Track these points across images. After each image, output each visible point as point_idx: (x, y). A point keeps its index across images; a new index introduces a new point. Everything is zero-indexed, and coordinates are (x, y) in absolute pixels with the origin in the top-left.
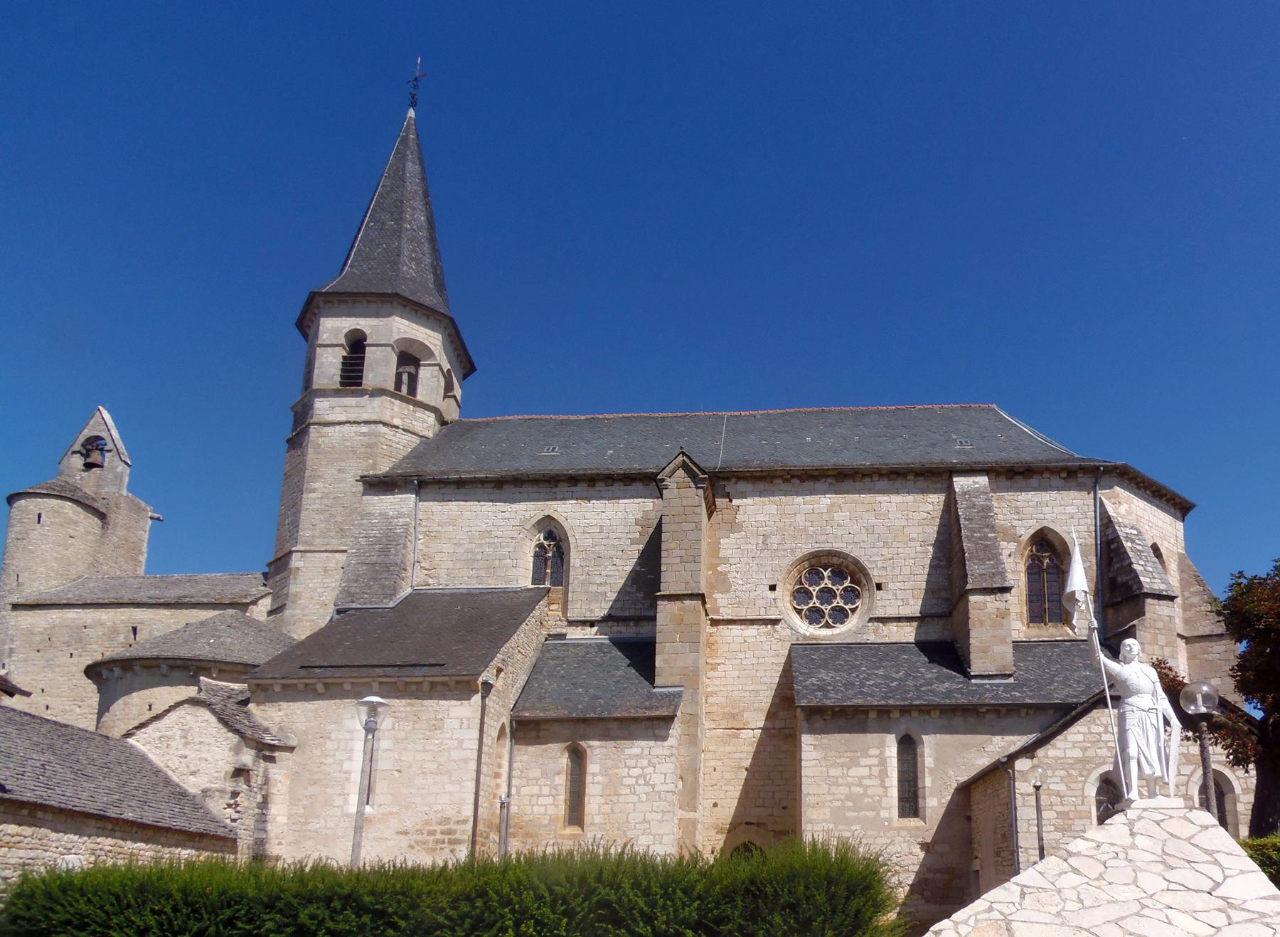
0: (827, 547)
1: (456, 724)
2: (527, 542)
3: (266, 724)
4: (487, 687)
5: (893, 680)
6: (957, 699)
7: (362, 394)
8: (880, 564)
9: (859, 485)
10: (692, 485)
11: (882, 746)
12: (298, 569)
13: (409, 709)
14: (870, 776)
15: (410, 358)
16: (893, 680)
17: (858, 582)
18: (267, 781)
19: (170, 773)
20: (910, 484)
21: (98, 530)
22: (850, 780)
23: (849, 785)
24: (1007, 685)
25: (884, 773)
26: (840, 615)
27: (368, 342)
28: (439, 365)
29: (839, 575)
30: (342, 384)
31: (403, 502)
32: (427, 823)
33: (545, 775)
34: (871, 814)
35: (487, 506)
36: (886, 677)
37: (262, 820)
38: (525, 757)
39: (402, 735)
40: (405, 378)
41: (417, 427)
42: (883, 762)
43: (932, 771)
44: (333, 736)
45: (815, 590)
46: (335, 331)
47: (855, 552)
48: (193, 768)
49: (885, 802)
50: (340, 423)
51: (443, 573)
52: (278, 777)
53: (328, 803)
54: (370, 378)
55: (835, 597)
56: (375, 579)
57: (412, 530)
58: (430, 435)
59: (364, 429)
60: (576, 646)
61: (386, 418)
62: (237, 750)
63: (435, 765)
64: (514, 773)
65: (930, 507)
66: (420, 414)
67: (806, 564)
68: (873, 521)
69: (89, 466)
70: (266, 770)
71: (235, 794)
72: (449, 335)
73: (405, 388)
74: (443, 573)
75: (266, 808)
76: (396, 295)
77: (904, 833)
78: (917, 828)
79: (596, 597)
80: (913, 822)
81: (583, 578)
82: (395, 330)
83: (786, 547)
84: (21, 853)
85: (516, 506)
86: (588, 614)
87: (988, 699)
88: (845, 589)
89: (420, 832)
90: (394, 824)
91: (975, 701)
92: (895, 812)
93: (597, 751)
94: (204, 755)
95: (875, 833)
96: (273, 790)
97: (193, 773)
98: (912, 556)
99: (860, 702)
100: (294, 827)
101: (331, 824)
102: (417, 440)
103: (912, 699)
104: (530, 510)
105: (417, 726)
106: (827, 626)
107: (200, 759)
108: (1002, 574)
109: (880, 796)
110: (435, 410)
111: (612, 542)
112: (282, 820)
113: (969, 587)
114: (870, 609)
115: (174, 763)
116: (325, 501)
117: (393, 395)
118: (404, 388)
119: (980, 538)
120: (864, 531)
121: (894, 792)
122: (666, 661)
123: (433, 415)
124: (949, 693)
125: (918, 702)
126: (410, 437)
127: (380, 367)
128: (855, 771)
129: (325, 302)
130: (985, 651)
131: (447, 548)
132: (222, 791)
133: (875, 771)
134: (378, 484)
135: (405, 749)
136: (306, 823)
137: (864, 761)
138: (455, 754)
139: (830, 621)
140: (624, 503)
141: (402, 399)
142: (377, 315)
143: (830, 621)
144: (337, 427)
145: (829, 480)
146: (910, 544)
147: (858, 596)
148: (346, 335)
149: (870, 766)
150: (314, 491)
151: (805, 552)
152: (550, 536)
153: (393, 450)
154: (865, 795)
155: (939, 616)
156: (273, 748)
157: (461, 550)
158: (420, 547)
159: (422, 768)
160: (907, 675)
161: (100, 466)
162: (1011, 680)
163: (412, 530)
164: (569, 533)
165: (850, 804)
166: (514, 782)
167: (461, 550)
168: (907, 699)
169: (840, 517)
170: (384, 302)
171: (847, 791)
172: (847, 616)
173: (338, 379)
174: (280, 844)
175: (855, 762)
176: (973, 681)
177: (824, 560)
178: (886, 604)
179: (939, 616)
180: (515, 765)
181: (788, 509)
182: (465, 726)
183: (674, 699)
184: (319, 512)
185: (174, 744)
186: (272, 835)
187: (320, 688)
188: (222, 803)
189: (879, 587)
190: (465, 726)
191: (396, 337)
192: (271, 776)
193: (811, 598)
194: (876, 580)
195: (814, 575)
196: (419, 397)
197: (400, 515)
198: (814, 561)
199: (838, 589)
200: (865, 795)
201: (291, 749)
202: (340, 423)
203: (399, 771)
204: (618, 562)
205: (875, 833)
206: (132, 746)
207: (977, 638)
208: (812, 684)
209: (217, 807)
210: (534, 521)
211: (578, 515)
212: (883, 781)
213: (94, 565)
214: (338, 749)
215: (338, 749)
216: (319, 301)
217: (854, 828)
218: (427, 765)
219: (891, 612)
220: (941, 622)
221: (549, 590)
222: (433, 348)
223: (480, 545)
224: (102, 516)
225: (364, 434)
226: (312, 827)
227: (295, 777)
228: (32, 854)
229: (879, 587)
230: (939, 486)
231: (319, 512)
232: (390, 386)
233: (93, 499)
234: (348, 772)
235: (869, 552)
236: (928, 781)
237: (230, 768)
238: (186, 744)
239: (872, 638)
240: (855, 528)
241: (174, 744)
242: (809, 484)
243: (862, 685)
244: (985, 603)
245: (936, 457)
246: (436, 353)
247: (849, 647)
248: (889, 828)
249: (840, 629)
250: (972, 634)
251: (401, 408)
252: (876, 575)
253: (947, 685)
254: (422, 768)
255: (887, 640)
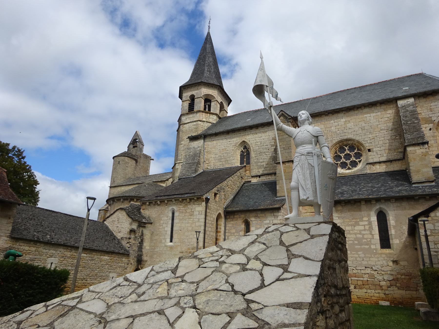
0: (345, 138)
1: (197, 213)
2: (238, 151)
3: (145, 215)
4: (207, 200)
5: (375, 187)
6: (404, 193)
7: (194, 113)
8: (369, 141)
9: (356, 112)
10: (286, 121)
11: (369, 216)
12: (177, 168)
13: (183, 208)
14: (365, 230)
15: (208, 100)
16: (375, 187)
17: (361, 150)
18: (142, 234)
19: (114, 232)
20: (378, 108)
21: (134, 165)
22: (356, 231)
23: (356, 234)
24: (431, 186)
25: (371, 228)
26: (354, 164)
27: (196, 97)
28: (217, 101)
29: (352, 148)
30: (189, 111)
31: (200, 143)
32: (189, 249)
33: (237, 232)
34: (367, 247)
35: (225, 141)
36: (372, 187)
37: (140, 247)
38: (230, 225)
39: (181, 218)
40: (207, 106)
41: (211, 120)
42: (370, 223)
43: (394, 227)
44: (162, 219)
45: (342, 155)
46: (187, 96)
47: (357, 138)
48: (119, 230)
49: (373, 241)
50: (188, 123)
51: (212, 164)
52: (147, 233)
53: (161, 242)
54: (196, 108)
55: (351, 157)
56: (190, 168)
57: (202, 151)
58: (215, 122)
59: (195, 123)
60: (253, 185)
61: (200, 120)
62: (131, 224)
63: (190, 228)
64: (226, 231)
65: (389, 115)
66: (211, 116)
67: (338, 145)
68: (364, 125)
69: (134, 147)
70: (142, 231)
71: (130, 238)
72: (219, 89)
73: (207, 109)
74: (212, 164)
75: (142, 244)
76: (202, 82)
77: (384, 256)
78: (390, 254)
79: (260, 167)
80: (387, 251)
81: (256, 161)
82: (202, 92)
83: (328, 140)
84: (31, 256)
85: (233, 140)
86: (258, 173)
87: (420, 192)
88: (355, 153)
89: (186, 252)
90: (179, 249)
91: (412, 193)
92: (379, 246)
93: (254, 222)
94: (122, 226)
95: (369, 255)
96: (145, 238)
97: (119, 232)
98: (383, 136)
99: (356, 197)
100: (151, 250)
101: (161, 249)
102: (210, 124)
103: (381, 195)
104: (236, 140)
105: (186, 214)
106: (349, 169)
107: (122, 228)
108: (423, 137)
109: (371, 239)
110: (216, 114)
111: (265, 147)
112: (147, 248)
113: (406, 144)
114: (367, 159)
115: (115, 229)
116: (185, 147)
117: (202, 112)
118: (207, 110)
119: (410, 124)
120: (360, 129)
121: (377, 237)
122: (280, 187)
123: (215, 116)
124: (399, 192)
125: (383, 196)
126: (208, 124)
127: (200, 104)
128: (357, 228)
129: (184, 89)
130: (418, 171)
131: (213, 156)
132: (126, 238)
133: (367, 227)
134: (193, 139)
135: (183, 223)
136: (155, 249)
137: (361, 223)
138: (197, 224)
139: (350, 167)
140: (267, 134)
141: (207, 113)
142: (198, 89)
143: (350, 167)
144: (188, 124)
145: (344, 112)
146: (381, 132)
147: (361, 155)
148: (190, 97)
149: (364, 225)
150: (182, 144)
151: (337, 141)
152: (245, 148)
153: (203, 127)
154: (363, 238)
155: (399, 160)
156: (145, 223)
157: (217, 156)
158: (205, 157)
159: (187, 229)
160: (382, 185)
161: (137, 147)
162: (434, 184)
163: (202, 151)
164: (251, 146)
165: (356, 242)
166: (227, 234)
167: (217, 156)
168: (378, 195)
169: (349, 125)
170: (199, 85)
171: (355, 236)
172: (357, 164)
173: (187, 110)
174: (147, 256)
175: (357, 224)
176: (414, 185)
177: (345, 143)
178: (373, 157)
179: (399, 160)
180: (227, 228)
181: (328, 126)
182: (200, 214)
183: (283, 201)
184: (183, 150)
185: (115, 223)
186: (144, 253)
187: (159, 202)
188: (126, 242)
189: (369, 150)
190: (200, 214)
191: (203, 94)
192: (144, 233)
193: (341, 158)
194: (368, 148)
195: (342, 149)
196: (211, 112)
197: (199, 147)
198: (341, 144)
199: (352, 154)
200: (363, 238)
201: (151, 223)
202: (188, 123)
203: (181, 230)
204: (267, 153)
205: (369, 255)
206: (105, 224)
207: (413, 167)
208: (339, 192)
209: (124, 243)
210: (239, 143)
211: (253, 139)
212: (371, 232)
213: (134, 174)
214: (164, 223)
215: (164, 223)
216: (182, 89)
217: (359, 253)
218: (189, 228)
219: (376, 160)
220: (400, 162)
221: (245, 166)
222: (214, 96)
223: (223, 154)
224: (136, 161)
225: (194, 125)
226: (156, 250)
227: (152, 234)
228: (36, 257)
229: (369, 150)
230: (392, 106)
231: (183, 150)
232: (202, 109)
233: (135, 156)
234: (166, 231)
235: (363, 137)
236: (392, 232)
237: (129, 230)
238: (118, 223)
239: (369, 172)
240: (356, 129)
241: (115, 223)
242: (336, 115)
243: (360, 191)
244: (415, 151)
245: (391, 96)
246: (216, 97)
247: (358, 176)
248: (376, 254)
249: (355, 169)
250: (410, 165)
251: (205, 115)
252: (367, 146)
253: (400, 188)
254: (187, 229)
255: (375, 172)
